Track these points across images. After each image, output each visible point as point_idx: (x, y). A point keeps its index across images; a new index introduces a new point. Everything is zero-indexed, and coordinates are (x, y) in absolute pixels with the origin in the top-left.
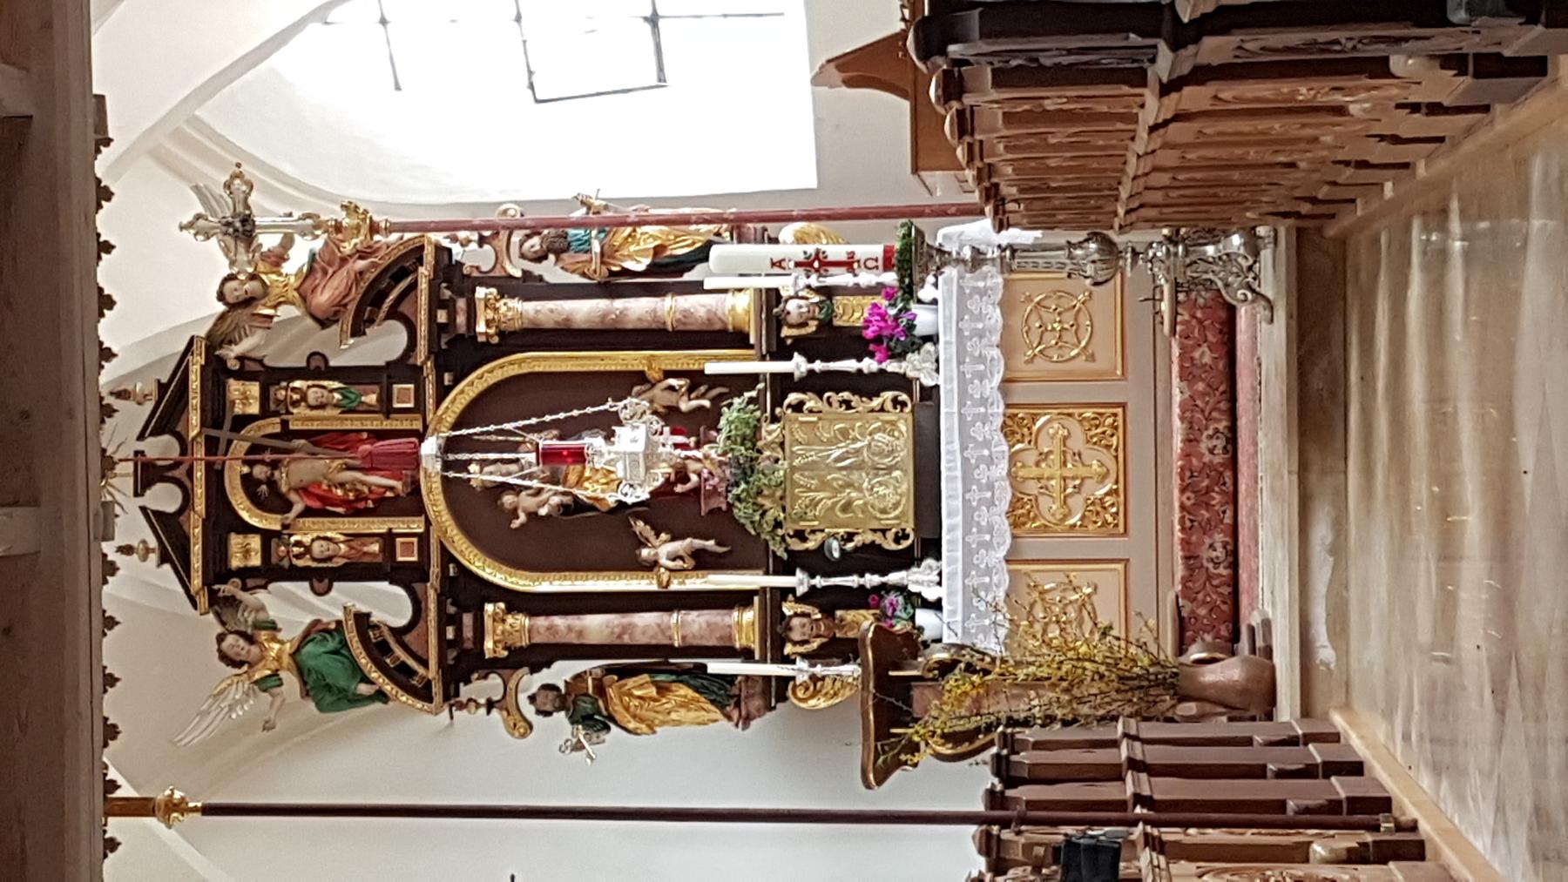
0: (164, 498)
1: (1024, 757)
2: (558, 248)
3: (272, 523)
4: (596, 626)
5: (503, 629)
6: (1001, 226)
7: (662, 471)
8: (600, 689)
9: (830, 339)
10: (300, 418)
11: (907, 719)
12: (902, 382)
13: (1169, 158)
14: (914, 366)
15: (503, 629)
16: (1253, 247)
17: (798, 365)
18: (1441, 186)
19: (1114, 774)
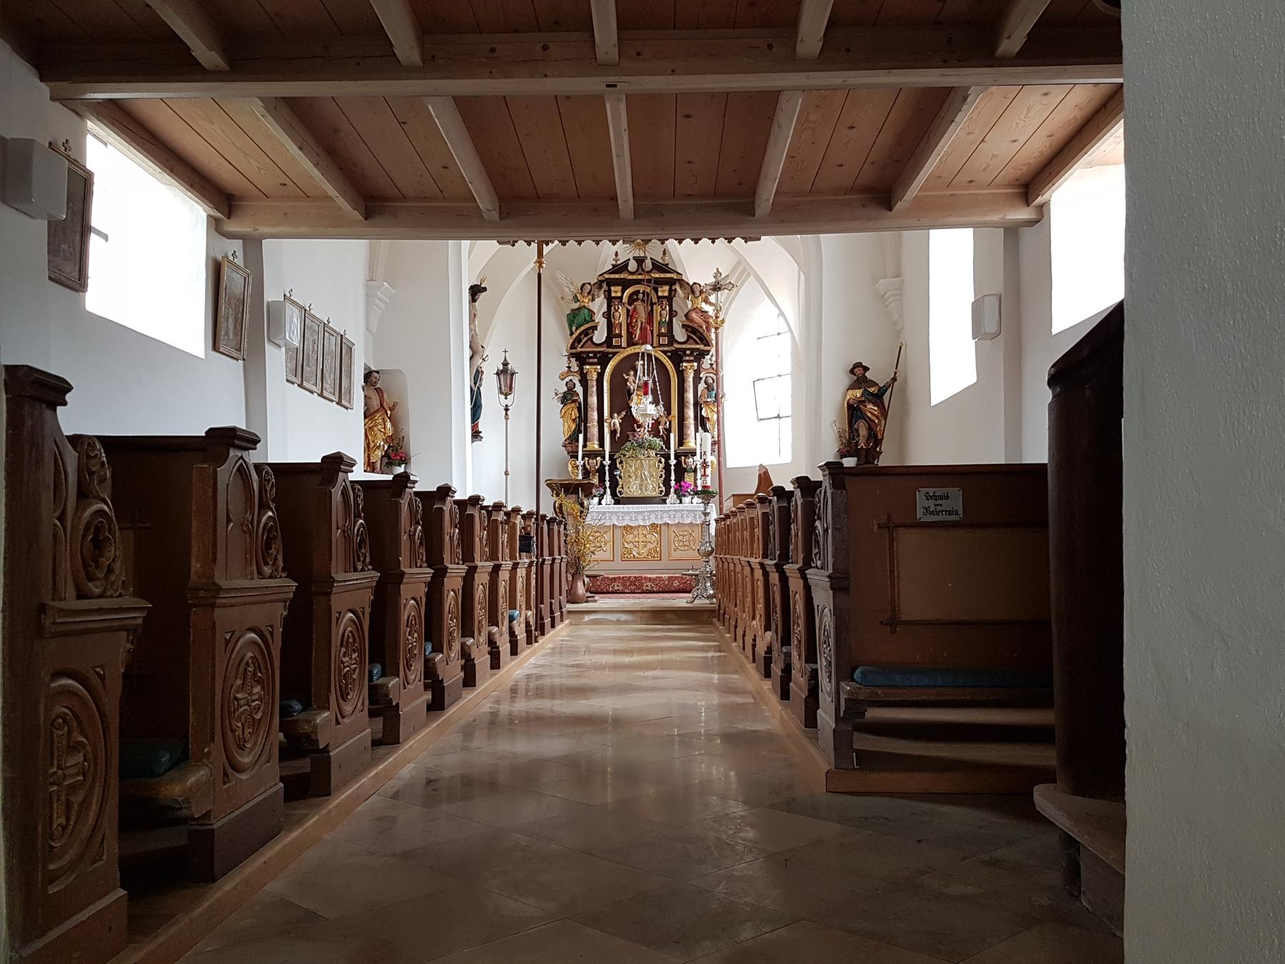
0: (633, 266)
1: (556, 527)
2: (709, 388)
3: (625, 299)
4: (593, 400)
5: (592, 371)
6: (717, 521)
7: (640, 419)
8: (574, 401)
9: (681, 471)
10: (657, 308)
11: (567, 493)
12: (667, 494)
13: (739, 568)
14: (672, 496)
15: (592, 371)
16: (709, 597)
17: (673, 461)
18: (730, 650)
19: (551, 554)
